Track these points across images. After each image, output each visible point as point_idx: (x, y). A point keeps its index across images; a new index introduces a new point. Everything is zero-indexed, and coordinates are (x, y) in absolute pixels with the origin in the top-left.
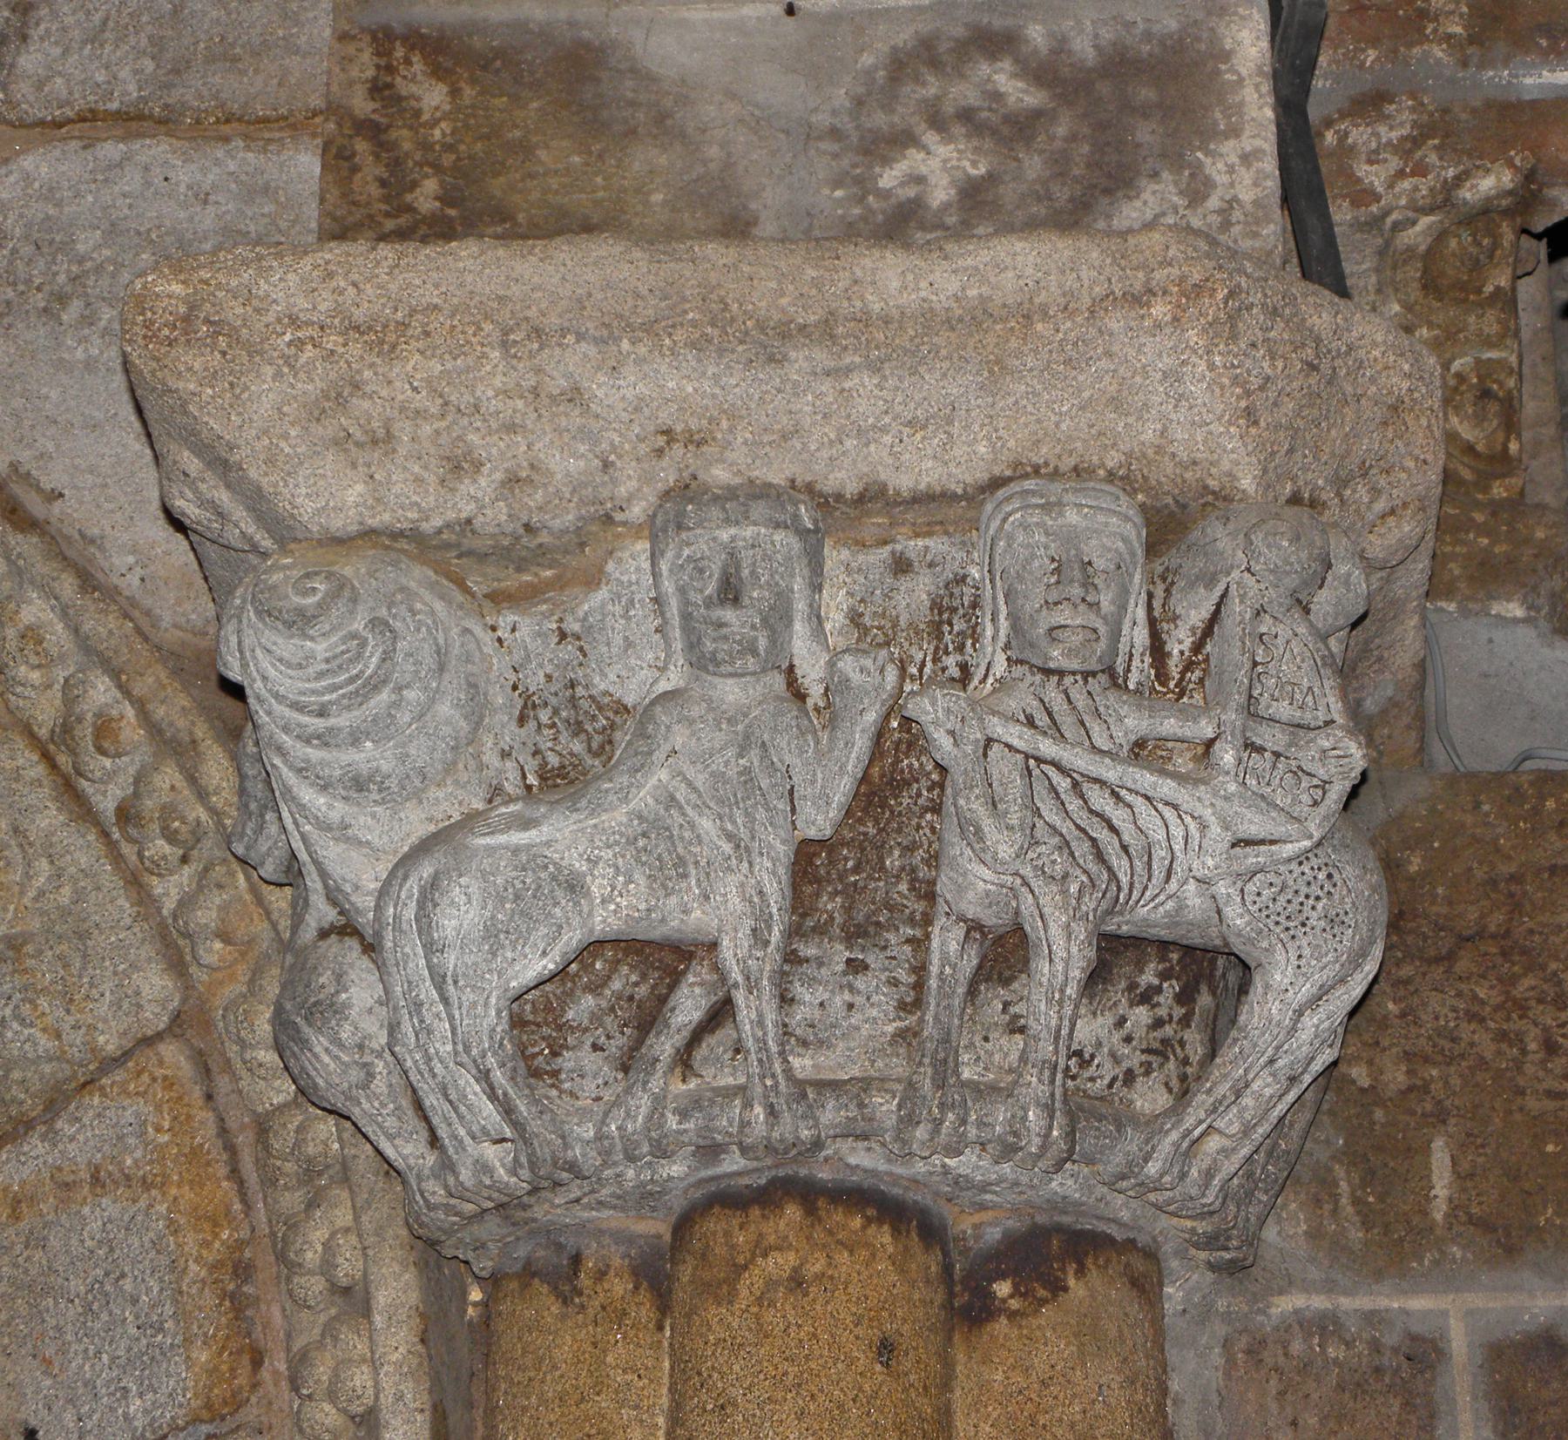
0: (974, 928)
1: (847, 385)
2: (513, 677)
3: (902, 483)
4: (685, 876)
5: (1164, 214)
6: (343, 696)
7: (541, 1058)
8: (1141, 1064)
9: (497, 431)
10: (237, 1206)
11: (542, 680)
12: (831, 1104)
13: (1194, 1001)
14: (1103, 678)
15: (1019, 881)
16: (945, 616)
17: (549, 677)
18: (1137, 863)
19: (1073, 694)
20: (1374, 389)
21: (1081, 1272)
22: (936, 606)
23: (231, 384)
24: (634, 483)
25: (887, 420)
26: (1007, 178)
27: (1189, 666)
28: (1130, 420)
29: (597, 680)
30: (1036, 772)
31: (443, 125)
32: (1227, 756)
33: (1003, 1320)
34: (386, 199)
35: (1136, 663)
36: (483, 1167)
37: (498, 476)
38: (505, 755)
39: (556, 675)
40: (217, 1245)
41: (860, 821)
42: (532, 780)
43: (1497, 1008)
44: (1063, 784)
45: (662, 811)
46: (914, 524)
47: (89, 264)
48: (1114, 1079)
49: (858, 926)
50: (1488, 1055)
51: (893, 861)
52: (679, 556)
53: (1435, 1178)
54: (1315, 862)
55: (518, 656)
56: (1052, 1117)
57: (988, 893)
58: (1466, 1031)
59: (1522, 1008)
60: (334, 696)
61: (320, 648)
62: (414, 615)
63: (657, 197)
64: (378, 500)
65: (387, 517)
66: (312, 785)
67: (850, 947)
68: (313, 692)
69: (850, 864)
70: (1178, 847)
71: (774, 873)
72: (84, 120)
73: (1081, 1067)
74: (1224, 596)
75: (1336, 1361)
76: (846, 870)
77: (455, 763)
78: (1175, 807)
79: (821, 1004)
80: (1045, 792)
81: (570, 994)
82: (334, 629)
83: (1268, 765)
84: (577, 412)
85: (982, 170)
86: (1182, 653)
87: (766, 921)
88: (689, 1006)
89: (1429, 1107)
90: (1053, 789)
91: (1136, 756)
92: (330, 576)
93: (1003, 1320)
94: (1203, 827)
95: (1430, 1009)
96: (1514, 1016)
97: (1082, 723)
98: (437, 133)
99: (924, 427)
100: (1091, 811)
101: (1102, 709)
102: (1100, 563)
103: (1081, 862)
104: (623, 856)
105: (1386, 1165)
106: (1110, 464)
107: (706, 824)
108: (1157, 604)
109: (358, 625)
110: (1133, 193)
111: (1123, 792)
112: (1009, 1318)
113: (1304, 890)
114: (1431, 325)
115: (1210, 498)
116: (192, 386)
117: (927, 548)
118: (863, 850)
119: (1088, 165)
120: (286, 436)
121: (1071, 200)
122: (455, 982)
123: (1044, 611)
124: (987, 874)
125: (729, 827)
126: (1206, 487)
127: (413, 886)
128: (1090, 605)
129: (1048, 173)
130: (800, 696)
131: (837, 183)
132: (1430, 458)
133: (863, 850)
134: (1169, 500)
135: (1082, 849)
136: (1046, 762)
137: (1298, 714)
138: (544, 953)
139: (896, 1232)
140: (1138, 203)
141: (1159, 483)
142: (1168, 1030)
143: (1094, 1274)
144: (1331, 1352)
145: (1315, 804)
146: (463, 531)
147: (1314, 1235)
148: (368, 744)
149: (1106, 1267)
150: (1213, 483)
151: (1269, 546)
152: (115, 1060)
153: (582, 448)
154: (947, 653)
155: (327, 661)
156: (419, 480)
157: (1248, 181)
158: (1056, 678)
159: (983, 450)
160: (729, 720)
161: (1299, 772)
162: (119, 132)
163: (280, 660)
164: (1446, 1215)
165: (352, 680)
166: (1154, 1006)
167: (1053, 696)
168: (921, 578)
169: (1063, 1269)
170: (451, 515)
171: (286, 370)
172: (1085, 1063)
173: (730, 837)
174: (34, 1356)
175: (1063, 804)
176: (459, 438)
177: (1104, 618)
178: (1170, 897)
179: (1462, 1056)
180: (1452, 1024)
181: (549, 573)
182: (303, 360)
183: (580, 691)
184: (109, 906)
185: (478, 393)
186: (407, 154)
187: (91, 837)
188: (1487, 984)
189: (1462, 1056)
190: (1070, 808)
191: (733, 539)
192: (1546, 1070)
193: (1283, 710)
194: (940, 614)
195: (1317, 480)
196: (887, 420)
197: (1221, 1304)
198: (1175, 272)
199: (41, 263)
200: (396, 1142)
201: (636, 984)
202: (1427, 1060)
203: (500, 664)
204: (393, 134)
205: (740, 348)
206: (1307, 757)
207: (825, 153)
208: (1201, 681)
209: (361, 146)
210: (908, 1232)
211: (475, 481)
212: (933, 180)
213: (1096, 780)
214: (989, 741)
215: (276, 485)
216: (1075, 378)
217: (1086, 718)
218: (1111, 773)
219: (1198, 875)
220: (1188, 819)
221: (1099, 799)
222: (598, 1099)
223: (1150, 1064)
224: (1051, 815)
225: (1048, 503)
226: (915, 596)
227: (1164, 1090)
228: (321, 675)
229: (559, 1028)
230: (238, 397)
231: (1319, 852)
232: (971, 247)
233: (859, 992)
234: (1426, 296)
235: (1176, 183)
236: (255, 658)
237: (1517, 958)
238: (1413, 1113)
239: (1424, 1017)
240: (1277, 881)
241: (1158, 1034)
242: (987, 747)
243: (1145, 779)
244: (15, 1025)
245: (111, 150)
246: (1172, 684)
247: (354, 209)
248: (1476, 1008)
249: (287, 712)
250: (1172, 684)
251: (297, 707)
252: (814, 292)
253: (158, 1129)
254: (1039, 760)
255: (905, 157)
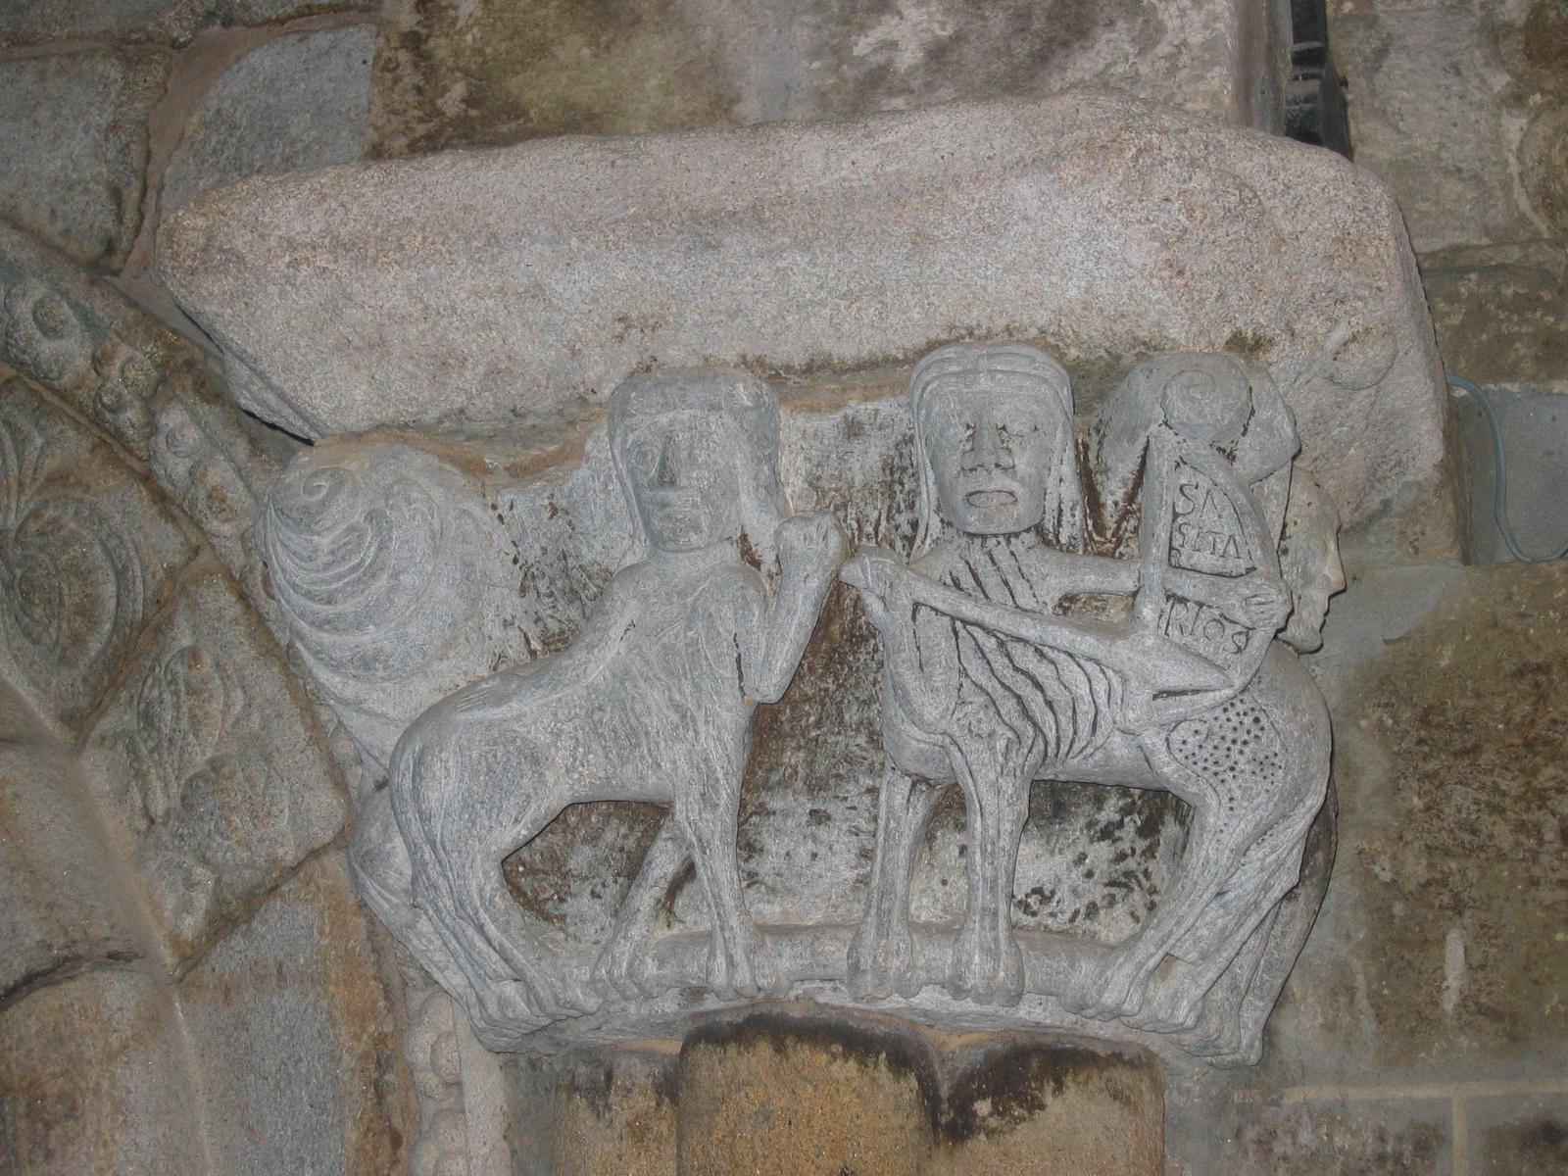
0: (919, 781)
1: (781, 264)
2: (513, 551)
3: (846, 351)
4: (638, 745)
5: (1115, 63)
6: (348, 584)
7: (550, 903)
8: (1104, 898)
9: (474, 330)
10: (382, 1003)
11: (539, 553)
12: (787, 952)
13: (1159, 832)
14: (1029, 538)
15: (948, 740)
16: (896, 476)
17: (544, 550)
18: (1062, 719)
19: (995, 552)
20: (1315, 224)
21: (1059, 1088)
22: (889, 467)
23: (246, 304)
24: (601, 367)
25: (823, 294)
26: (972, 37)
27: (1124, 516)
28: (1054, 279)
29: (585, 551)
30: (962, 633)
31: (475, 30)
32: (1148, 612)
33: (982, 1137)
34: (419, 105)
35: (1066, 517)
36: (503, 1002)
37: (481, 369)
38: (507, 624)
39: (549, 548)
40: (365, 1037)
41: (821, 677)
42: (536, 645)
43: (1517, 799)
44: (989, 644)
45: (618, 685)
46: (865, 388)
47: (300, 145)
48: (1076, 913)
49: (821, 779)
50: (1506, 846)
51: (851, 716)
52: (625, 441)
53: (1447, 970)
54: (1240, 708)
55: (516, 531)
56: (997, 960)
57: (921, 751)
58: (1487, 820)
59: (1541, 798)
60: (341, 584)
61: (324, 542)
62: (410, 504)
63: (653, 83)
64: (383, 397)
65: (391, 412)
66: (327, 665)
67: (813, 799)
68: (323, 581)
69: (812, 719)
70: (1102, 699)
71: (719, 739)
72: (301, 15)
73: (1041, 902)
74: (1146, 449)
75: (1341, 1150)
76: (807, 726)
77: (455, 638)
78: (1097, 662)
79: (788, 854)
80: (971, 654)
81: (571, 845)
82: (335, 523)
83: (1191, 615)
84: (541, 306)
85: (949, 31)
86: (1116, 504)
87: (713, 786)
88: (663, 863)
89: (1446, 899)
90: (979, 648)
91: (1066, 610)
92: (334, 473)
93: (982, 1137)
94: (1125, 681)
95: (1453, 803)
96: (1534, 806)
97: (1006, 583)
98: (469, 38)
99: (858, 299)
100: (1016, 669)
101: (1024, 569)
102: (1015, 427)
103: (1006, 719)
104: (583, 729)
105: (1402, 958)
106: (1041, 323)
107: (656, 696)
108: (1092, 456)
109: (358, 518)
110: (1088, 44)
111: (1046, 650)
112: (987, 1135)
113: (1230, 736)
114: (1543, 93)
115: (1142, 348)
116: (214, 308)
117: (877, 411)
118: (823, 705)
119: (1049, 18)
120: (297, 346)
121: (1031, 55)
122: (444, 848)
123: (962, 479)
124: (919, 734)
125: (677, 697)
126: (1135, 339)
127: (408, 759)
128: (1005, 469)
129: (1011, 30)
130: (756, 564)
131: (816, 55)
132: (1383, 284)
133: (823, 705)
134: (1102, 353)
135: (1009, 706)
136: (972, 624)
137: (1221, 562)
138: (516, 821)
139: (862, 1064)
140: (1092, 54)
141: (1090, 338)
142: (1131, 864)
143: (1072, 1091)
144: (1338, 1141)
145: (1239, 650)
146: (460, 420)
147: (1330, 1027)
148: (371, 627)
149: (1086, 1083)
150: (1142, 334)
151: (1183, 399)
152: (293, 869)
153: (551, 339)
154: (899, 511)
155: (333, 552)
156: (413, 377)
157: (1197, 25)
158: (978, 541)
159: (916, 316)
160: (679, 594)
161: (1223, 620)
162: (330, 23)
163: (294, 553)
164: (1457, 1006)
165: (354, 569)
166: (1115, 841)
167: (978, 557)
168: (872, 440)
169: (1041, 1088)
170: (445, 407)
171: (289, 288)
172: (1045, 899)
173: (678, 708)
174: (242, 1124)
175: (989, 663)
176: (442, 337)
177: (1022, 482)
178: (1097, 749)
179: (1482, 848)
180: (1473, 817)
181: (553, 448)
182: (299, 280)
183: (571, 562)
184: (287, 732)
185: (453, 296)
186: (441, 60)
187: (275, 670)
188: (1509, 776)
189: (1482, 848)
190: (995, 666)
191: (672, 423)
192: (1561, 859)
193: (1205, 560)
194: (892, 474)
195: (1256, 318)
196: (823, 294)
197: (1237, 1096)
198: (1084, 134)
199: (262, 147)
200: (446, 973)
201: (625, 837)
202: (1447, 853)
203: (502, 539)
204: (432, 43)
205: (679, 238)
206: (1232, 601)
207: (807, 25)
208: (1136, 529)
209: (404, 56)
210: (876, 1065)
211: (461, 375)
212: (903, 45)
213: (1019, 639)
214: (917, 606)
215: (295, 391)
216: (996, 243)
217: (1010, 579)
218: (1028, 630)
219: (1122, 727)
220: (1110, 673)
221: (1027, 660)
222: (597, 942)
223: (1113, 896)
224: (976, 670)
225: (963, 371)
226: (867, 460)
227: (1130, 919)
228: (327, 566)
229: (564, 876)
230: (253, 315)
231: (1246, 697)
232: (892, 123)
233: (822, 842)
234: (1533, 66)
235: (1129, 31)
236: (276, 552)
237: (1540, 748)
238: (1431, 907)
239: (1447, 810)
240: (1203, 728)
241: (1121, 867)
242: (915, 611)
243: (1062, 635)
244: (218, 839)
245: (321, 41)
246: (1109, 534)
247: (392, 117)
248: (1497, 800)
249: (303, 601)
250: (1109, 534)
251: (310, 596)
252: (744, 179)
253: (321, 933)
254: (965, 622)
255: (880, 23)
